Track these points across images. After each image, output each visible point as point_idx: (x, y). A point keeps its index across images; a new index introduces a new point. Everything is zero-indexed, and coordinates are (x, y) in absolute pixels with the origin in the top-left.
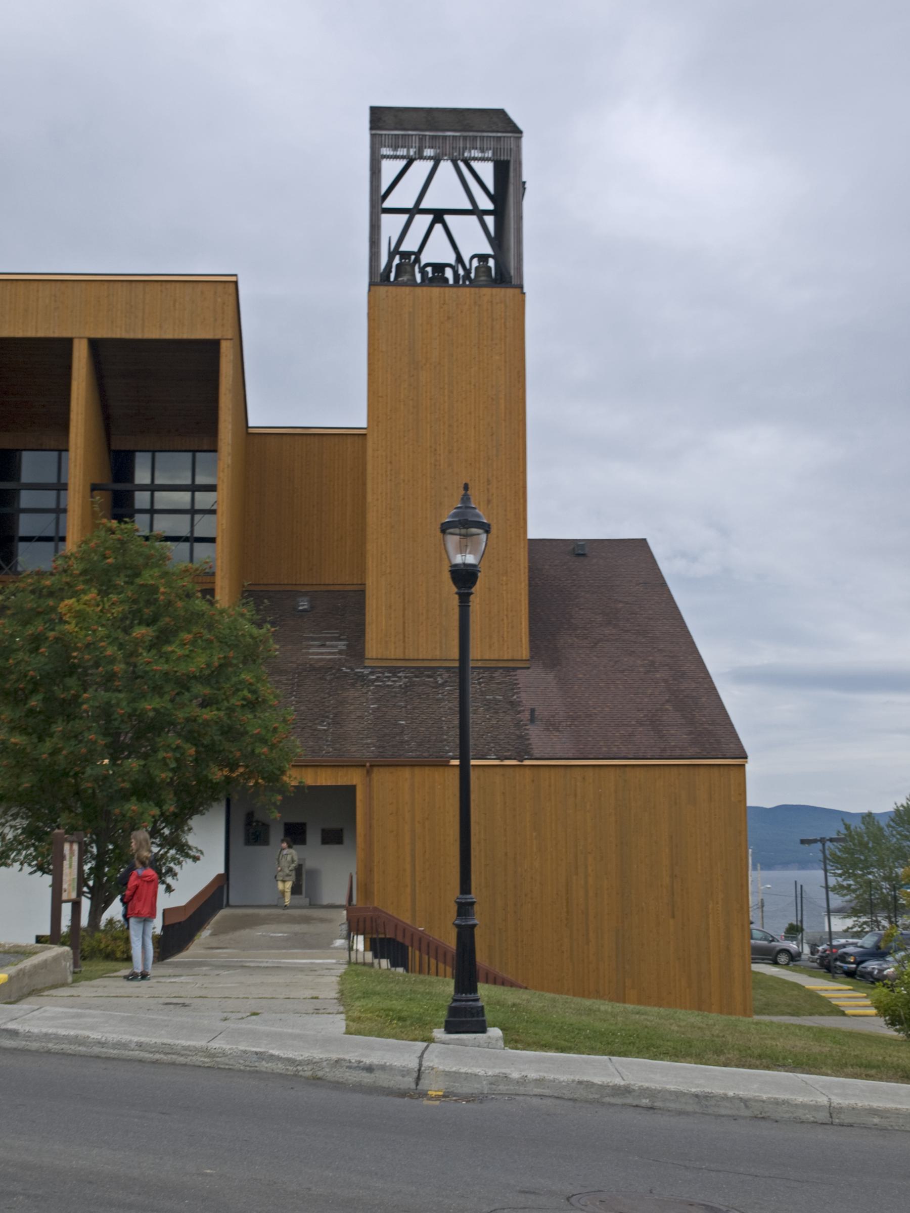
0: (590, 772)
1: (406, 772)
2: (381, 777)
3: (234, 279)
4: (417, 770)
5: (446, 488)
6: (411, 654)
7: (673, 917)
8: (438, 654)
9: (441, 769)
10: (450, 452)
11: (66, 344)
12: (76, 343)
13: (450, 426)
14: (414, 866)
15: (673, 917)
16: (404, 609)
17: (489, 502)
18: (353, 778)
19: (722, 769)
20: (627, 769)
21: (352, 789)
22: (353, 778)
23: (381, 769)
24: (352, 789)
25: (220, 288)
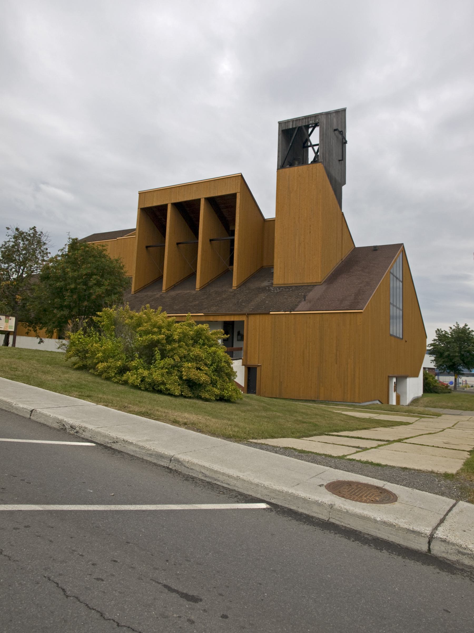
0: (311, 316)
1: (258, 317)
2: (251, 318)
3: (240, 174)
4: (261, 316)
5: (298, 230)
6: (286, 282)
7: (336, 364)
8: (294, 282)
9: (268, 315)
10: (299, 218)
11: (199, 200)
12: (201, 199)
13: (299, 210)
14: (259, 345)
15: (336, 364)
16: (284, 268)
17: (310, 232)
18: (244, 318)
19: (355, 314)
20: (324, 315)
21: (243, 322)
22: (244, 318)
23: (251, 316)
24: (243, 322)
25: (237, 177)
